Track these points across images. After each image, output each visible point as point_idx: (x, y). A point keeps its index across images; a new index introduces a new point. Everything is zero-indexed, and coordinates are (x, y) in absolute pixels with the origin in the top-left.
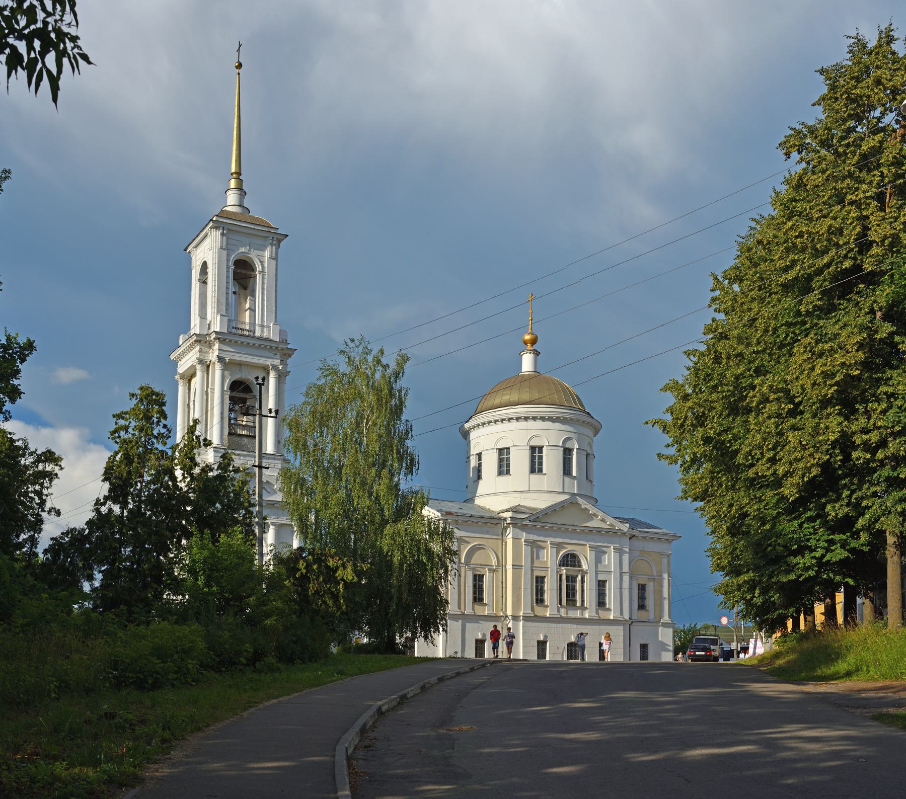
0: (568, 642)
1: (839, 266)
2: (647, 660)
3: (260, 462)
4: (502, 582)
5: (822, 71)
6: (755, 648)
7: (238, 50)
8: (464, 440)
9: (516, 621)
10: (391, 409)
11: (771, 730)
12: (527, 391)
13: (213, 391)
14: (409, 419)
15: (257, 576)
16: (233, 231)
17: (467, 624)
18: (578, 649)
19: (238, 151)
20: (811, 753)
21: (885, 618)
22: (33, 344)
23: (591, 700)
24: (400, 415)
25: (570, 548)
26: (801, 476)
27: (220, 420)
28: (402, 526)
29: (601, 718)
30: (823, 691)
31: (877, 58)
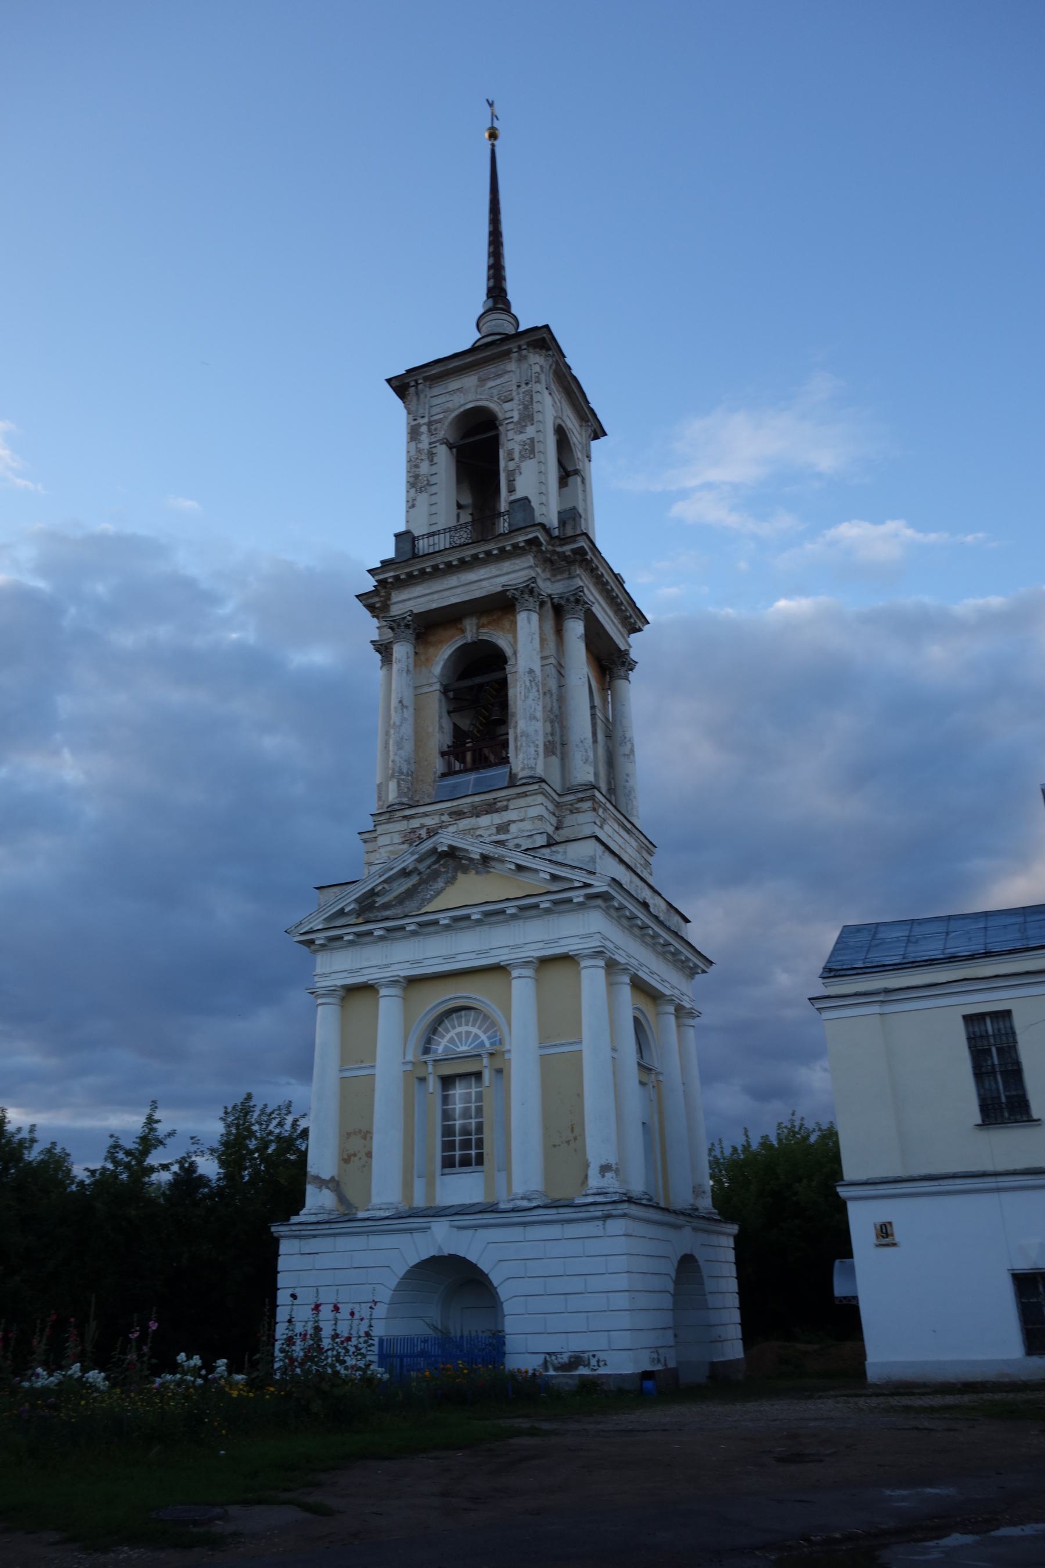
1: (311, 1351)
8: (455, 722)
9: (430, 1050)
12: (418, 543)
13: (544, 499)
18: (567, 573)
20: (633, 937)
25: (471, 631)
27: (652, 891)
29: (434, 372)
30: (454, 384)
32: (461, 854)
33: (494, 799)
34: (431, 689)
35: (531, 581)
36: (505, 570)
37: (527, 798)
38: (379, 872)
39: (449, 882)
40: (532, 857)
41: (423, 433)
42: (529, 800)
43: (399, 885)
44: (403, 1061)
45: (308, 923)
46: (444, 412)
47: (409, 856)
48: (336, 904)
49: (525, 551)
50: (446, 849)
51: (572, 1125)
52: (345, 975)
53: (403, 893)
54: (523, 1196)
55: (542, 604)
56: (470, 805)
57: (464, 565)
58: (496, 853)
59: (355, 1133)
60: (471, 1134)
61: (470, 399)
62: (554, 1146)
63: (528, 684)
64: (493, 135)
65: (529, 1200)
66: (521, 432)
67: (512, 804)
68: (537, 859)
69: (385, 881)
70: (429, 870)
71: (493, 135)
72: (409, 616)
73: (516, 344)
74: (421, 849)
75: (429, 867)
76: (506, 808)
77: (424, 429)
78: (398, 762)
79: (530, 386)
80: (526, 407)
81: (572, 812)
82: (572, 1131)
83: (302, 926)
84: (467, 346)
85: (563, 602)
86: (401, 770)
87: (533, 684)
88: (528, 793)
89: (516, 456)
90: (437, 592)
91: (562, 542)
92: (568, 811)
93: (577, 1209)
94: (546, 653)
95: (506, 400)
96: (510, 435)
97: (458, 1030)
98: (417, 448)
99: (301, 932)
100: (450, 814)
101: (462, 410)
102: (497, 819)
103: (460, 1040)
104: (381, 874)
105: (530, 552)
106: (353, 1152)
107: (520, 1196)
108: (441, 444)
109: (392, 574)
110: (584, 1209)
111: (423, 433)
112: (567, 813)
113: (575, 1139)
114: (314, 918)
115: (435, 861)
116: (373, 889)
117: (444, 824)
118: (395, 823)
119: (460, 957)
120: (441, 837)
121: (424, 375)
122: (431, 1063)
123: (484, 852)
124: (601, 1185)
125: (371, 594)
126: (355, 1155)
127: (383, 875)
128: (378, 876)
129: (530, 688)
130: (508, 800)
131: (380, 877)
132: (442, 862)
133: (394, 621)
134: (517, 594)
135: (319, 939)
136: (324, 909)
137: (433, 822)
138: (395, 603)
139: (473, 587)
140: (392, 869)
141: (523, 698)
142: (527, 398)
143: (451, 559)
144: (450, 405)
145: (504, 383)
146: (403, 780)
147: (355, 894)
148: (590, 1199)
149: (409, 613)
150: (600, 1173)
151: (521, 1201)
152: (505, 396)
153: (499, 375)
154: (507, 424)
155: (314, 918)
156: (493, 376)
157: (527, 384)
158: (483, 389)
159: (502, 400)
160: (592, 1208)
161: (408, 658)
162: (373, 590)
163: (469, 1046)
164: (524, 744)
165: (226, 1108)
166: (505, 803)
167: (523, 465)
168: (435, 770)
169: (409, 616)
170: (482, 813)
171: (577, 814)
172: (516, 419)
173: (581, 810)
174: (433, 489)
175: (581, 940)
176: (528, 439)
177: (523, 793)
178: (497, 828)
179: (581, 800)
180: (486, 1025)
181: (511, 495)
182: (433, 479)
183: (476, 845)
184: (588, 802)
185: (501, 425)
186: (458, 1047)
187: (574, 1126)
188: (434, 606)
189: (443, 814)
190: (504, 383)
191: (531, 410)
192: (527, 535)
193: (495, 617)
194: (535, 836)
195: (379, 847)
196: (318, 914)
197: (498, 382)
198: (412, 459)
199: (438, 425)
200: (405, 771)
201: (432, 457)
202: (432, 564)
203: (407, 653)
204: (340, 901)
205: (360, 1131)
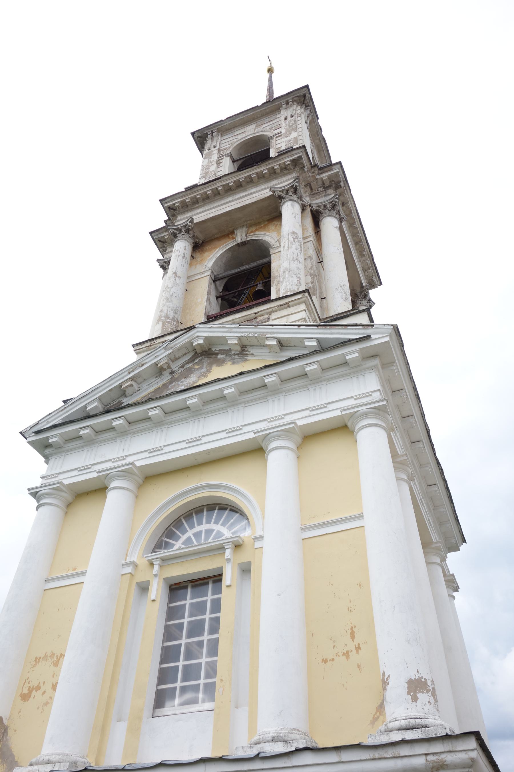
0: (136, 582)
10: (293, 185)
19: (230, 275)
21: (29, 767)
22: (53, 690)
23: (424, 509)
24: (179, 214)
25: (240, 237)
28: (300, 250)
32: (218, 349)
33: (255, 314)
38: (129, 368)
39: (202, 375)
40: (297, 327)
43: (149, 385)
44: (123, 562)
47: (163, 351)
49: (291, 171)
50: (202, 342)
51: (352, 628)
52: (76, 473)
53: (152, 392)
54: (275, 735)
57: (239, 186)
60: (205, 685)
62: (325, 661)
64: (270, 70)
65: (286, 741)
68: (302, 327)
69: (132, 379)
70: (182, 369)
71: (270, 70)
73: (285, 100)
74: (176, 344)
75: (182, 367)
82: (353, 637)
91: (320, 172)
93: (377, 754)
94: (306, 235)
97: (197, 529)
104: (131, 370)
105: (294, 171)
106: (35, 685)
107: (271, 735)
110: (390, 752)
113: (358, 648)
115: (191, 358)
119: (204, 440)
120: (198, 332)
122: (158, 562)
124: (413, 714)
125: (163, 230)
126: (38, 688)
127: (133, 371)
128: (127, 372)
129: (293, 242)
131: (129, 373)
132: (196, 361)
135: (53, 436)
140: (143, 365)
146: (167, 322)
148: (396, 737)
150: (408, 693)
151: (273, 743)
157: (292, 116)
160: (404, 751)
161: (185, 249)
162: (164, 227)
165: (14, 752)
177: (285, 304)
183: (234, 330)
187: (354, 629)
192: (293, 156)
193: (262, 226)
196: (58, 413)
200: (171, 317)
203: (185, 247)
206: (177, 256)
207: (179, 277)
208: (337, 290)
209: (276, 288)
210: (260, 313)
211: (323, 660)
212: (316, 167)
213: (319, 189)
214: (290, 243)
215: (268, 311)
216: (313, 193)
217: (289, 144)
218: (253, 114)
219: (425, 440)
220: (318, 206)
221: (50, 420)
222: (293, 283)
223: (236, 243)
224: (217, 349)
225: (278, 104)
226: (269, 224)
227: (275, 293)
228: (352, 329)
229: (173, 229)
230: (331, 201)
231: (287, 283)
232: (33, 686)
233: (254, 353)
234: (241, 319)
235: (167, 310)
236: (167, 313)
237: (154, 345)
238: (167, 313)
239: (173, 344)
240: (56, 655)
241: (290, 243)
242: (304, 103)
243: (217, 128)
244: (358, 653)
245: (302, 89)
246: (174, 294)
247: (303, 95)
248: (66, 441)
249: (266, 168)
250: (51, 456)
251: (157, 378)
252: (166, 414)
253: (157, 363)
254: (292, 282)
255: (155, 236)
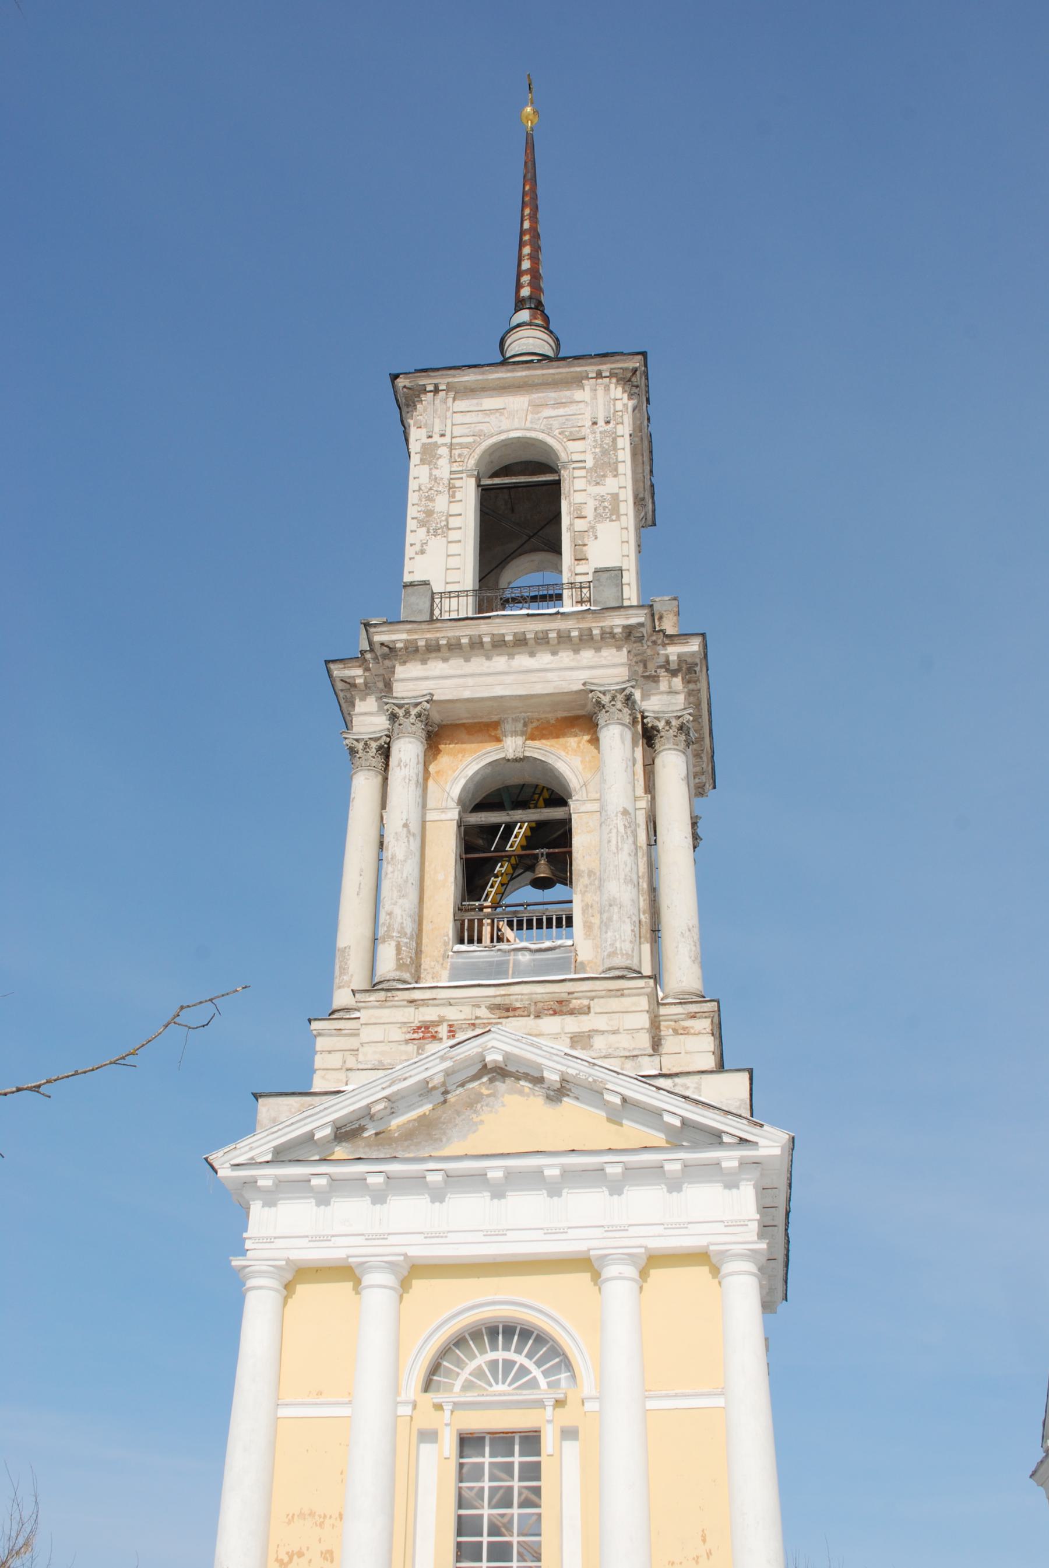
2: (537, 928)
3: (462, 446)
4: (552, 1048)
5: (301, 1548)
6: (535, 430)
7: (207, 1025)
11: (568, 1325)
14: (596, 541)
15: (531, 237)
16: (618, 683)
17: (404, 581)
25: (512, 746)
26: (498, 414)
30: (490, 402)
31: (613, 705)
34: (443, 817)
35: (630, 684)
36: (585, 662)
37: (623, 999)
40: (654, 1089)
41: (441, 456)
42: (626, 1002)
45: (247, 1148)
46: (474, 435)
47: (438, 1061)
48: (303, 1123)
50: (500, 1058)
53: (414, 1120)
55: (634, 721)
56: (526, 997)
58: (590, 1075)
59: (302, 1516)
61: (517, 425)
63: (622, 829)
66: (598, 484)
67: (596, 1006)
68: (661, 1091)
72: (427, 702)
73: (596, 368)
76: (587, 1011)
77: (444, 451)
78: (399, 917)
79: (611, 425)
80: (605, 452)
81: (676, 1032)
82: (704, 1541)
83: (237, 1152)
84: (499, 361)
85: (661, 725)
86: (402, 928)
87: (629, 831)
88: (626, 992)
89: (589, 511)
90: (473, 675)
92: (671, 1031)
95: (571, 438)
96: (579, 484)
98: (431, 475)
99: (232, 1162)
100: (494, 1008)
101: (503, 437)
102: (572, 1024)
103: (516, 1379)
108: (468, 476)
109: (404, 636)
111: (441, 456)
112: (669, 1034)
113: (709, 1554)
114: (258, 1143)
116: (368, 1107)
117: (477, 1021)
118: (394, 1010)
120: (494, 1039)
121: (450, 380)
123: (570, 1071)
126: (300, 1554)
129: (625, 837)
130: (592, 999)
131: (383, 1089)
133: (400, 706)
134: (605, 700)
135: (264, 1177)
136: (279, 1130)
137: (462, 1016)
138: (403, 680)
139: (534, 677)
141: (613, 848)
142: (608, 440)
143: (503, 631)
144: (483, 427)
145: (569, 415)
147: (336, 1111)
149: (428, 698)
152: (571, 432)
153: (562, 403)
154: (574, 468)
155: (258, 1143)
156: (552, 402)
158: (536, 416)
159: (566, 437)
163: (509, 1385)
164: (615, 917)
166: (586, 1002)
167: (599, 527)
168: (446, 938)
169: (427, 702)
170: (546, 1012)
171: (686, 1036)
172: (590, 464)
173: (692, 1031)
174: (453, 535)
175: (312, 1243)
176: (608, 494)
178: (571, 1038)
179: (693, 1016)
180: (544, 1349)
181: (578, 565)
182: (454, 522)
184: (704, 1020)
185: (565, 468)
186: (491, 1385)
188: (467, 694)
189: (479, 1006)
190: (569, 415)
191: (615, 457)
194: (640, 1058)
195: (362, 1044)
197: (561, 411)
198: (423, 488)
199: (466, 451)
201: (454, 492)
202: (471, 633)
204: (310, 1119)
205: (312, 1514)
206: (407, 781)
207: (414, 835)
208: (683, 936)
209: (582, 901)
210: (576, 995)
211: (669, 1562)
212: (661, 633)
213: (658, 670)
214: (619, 838)
215: (589, 994)
216: (647, 674)
217: (601, 508)
218: (526, 376)
219: (782, 1227)
220: (656, 718)
221: (254, 1145)
222: (626, 937)
223: (502, 755)
224: (520, 1071)
225: (580, 372)
226: (566, 730)
227: (581, 912)
228: (734, 1121)
229: (394, 704)
230: (679, 714)
231: (616, 934)
232: (293, 1551)
233: (580, 1098)
234: (544, 995)
235: (402, 916)
236: (402, 923)
237: (392, 1001)
238: (402, 923)
239: (454, 1053)
240: (317, 1514)
241: (619, 838)
242: (629, 380)
243: (448, 383)
244: (708, 1558)
245: (632, 357)
246: (409, 878)
247: (632, 369)
248: (280, 1182)
249: (577, 626)
250: (254, 1201)
251: (421, 1098)
252: (450, 1179)
253: (428, 1080)
254: (624, 936)
255: (336, 669)
